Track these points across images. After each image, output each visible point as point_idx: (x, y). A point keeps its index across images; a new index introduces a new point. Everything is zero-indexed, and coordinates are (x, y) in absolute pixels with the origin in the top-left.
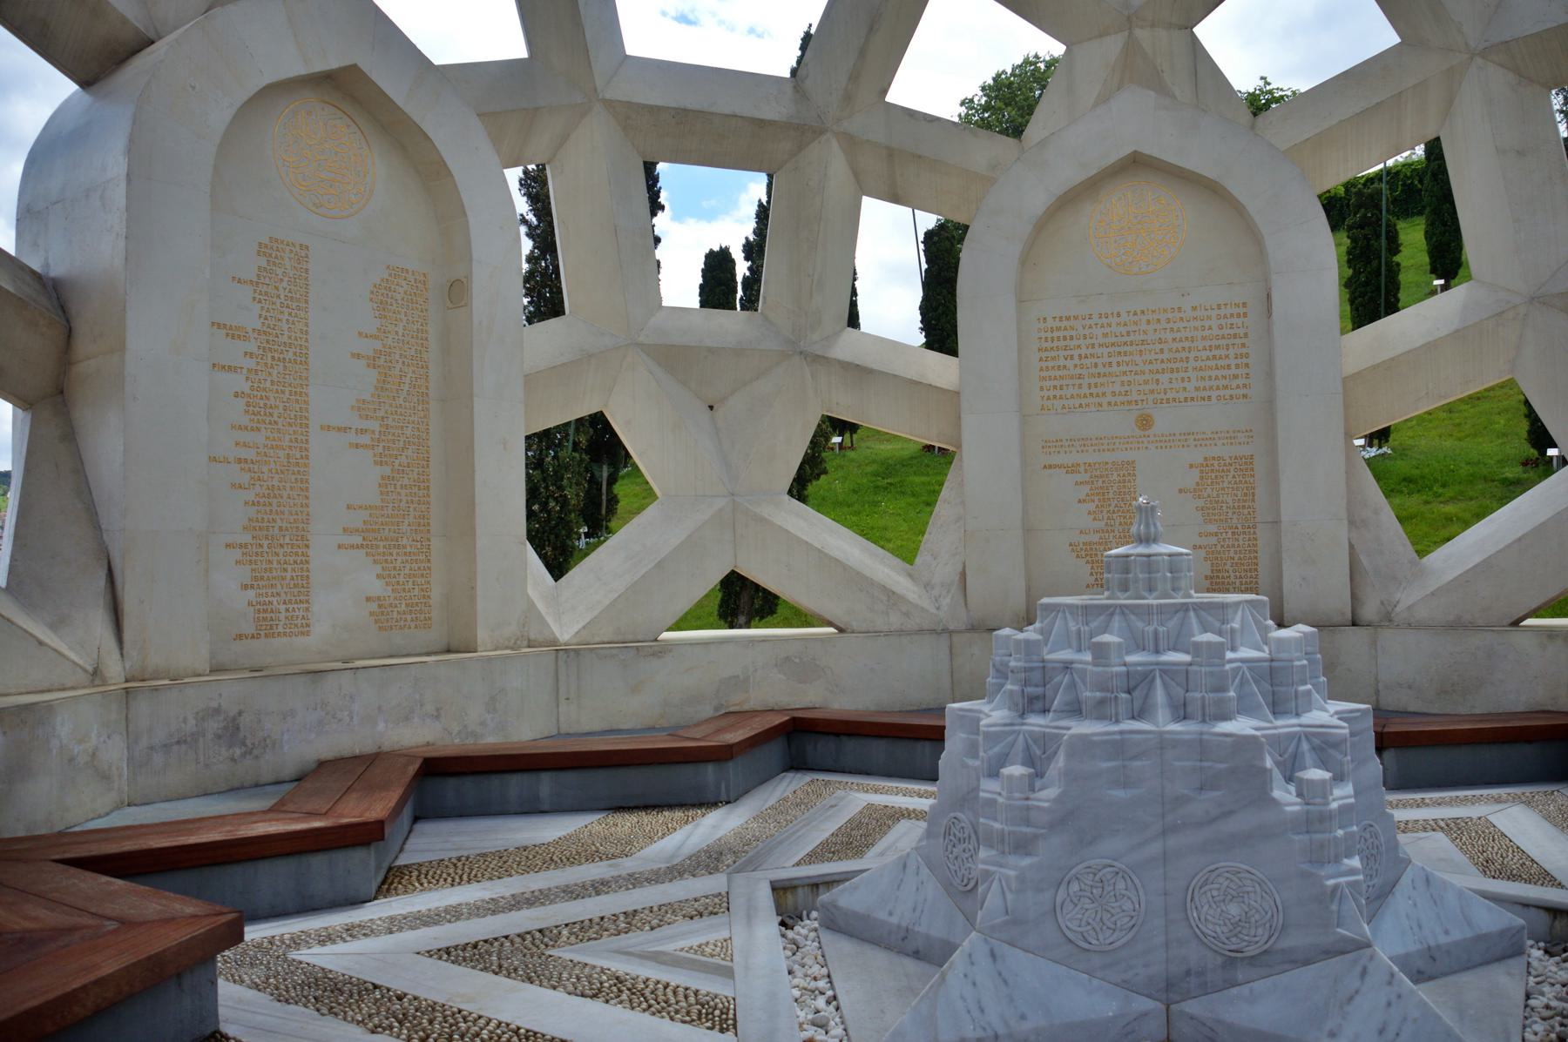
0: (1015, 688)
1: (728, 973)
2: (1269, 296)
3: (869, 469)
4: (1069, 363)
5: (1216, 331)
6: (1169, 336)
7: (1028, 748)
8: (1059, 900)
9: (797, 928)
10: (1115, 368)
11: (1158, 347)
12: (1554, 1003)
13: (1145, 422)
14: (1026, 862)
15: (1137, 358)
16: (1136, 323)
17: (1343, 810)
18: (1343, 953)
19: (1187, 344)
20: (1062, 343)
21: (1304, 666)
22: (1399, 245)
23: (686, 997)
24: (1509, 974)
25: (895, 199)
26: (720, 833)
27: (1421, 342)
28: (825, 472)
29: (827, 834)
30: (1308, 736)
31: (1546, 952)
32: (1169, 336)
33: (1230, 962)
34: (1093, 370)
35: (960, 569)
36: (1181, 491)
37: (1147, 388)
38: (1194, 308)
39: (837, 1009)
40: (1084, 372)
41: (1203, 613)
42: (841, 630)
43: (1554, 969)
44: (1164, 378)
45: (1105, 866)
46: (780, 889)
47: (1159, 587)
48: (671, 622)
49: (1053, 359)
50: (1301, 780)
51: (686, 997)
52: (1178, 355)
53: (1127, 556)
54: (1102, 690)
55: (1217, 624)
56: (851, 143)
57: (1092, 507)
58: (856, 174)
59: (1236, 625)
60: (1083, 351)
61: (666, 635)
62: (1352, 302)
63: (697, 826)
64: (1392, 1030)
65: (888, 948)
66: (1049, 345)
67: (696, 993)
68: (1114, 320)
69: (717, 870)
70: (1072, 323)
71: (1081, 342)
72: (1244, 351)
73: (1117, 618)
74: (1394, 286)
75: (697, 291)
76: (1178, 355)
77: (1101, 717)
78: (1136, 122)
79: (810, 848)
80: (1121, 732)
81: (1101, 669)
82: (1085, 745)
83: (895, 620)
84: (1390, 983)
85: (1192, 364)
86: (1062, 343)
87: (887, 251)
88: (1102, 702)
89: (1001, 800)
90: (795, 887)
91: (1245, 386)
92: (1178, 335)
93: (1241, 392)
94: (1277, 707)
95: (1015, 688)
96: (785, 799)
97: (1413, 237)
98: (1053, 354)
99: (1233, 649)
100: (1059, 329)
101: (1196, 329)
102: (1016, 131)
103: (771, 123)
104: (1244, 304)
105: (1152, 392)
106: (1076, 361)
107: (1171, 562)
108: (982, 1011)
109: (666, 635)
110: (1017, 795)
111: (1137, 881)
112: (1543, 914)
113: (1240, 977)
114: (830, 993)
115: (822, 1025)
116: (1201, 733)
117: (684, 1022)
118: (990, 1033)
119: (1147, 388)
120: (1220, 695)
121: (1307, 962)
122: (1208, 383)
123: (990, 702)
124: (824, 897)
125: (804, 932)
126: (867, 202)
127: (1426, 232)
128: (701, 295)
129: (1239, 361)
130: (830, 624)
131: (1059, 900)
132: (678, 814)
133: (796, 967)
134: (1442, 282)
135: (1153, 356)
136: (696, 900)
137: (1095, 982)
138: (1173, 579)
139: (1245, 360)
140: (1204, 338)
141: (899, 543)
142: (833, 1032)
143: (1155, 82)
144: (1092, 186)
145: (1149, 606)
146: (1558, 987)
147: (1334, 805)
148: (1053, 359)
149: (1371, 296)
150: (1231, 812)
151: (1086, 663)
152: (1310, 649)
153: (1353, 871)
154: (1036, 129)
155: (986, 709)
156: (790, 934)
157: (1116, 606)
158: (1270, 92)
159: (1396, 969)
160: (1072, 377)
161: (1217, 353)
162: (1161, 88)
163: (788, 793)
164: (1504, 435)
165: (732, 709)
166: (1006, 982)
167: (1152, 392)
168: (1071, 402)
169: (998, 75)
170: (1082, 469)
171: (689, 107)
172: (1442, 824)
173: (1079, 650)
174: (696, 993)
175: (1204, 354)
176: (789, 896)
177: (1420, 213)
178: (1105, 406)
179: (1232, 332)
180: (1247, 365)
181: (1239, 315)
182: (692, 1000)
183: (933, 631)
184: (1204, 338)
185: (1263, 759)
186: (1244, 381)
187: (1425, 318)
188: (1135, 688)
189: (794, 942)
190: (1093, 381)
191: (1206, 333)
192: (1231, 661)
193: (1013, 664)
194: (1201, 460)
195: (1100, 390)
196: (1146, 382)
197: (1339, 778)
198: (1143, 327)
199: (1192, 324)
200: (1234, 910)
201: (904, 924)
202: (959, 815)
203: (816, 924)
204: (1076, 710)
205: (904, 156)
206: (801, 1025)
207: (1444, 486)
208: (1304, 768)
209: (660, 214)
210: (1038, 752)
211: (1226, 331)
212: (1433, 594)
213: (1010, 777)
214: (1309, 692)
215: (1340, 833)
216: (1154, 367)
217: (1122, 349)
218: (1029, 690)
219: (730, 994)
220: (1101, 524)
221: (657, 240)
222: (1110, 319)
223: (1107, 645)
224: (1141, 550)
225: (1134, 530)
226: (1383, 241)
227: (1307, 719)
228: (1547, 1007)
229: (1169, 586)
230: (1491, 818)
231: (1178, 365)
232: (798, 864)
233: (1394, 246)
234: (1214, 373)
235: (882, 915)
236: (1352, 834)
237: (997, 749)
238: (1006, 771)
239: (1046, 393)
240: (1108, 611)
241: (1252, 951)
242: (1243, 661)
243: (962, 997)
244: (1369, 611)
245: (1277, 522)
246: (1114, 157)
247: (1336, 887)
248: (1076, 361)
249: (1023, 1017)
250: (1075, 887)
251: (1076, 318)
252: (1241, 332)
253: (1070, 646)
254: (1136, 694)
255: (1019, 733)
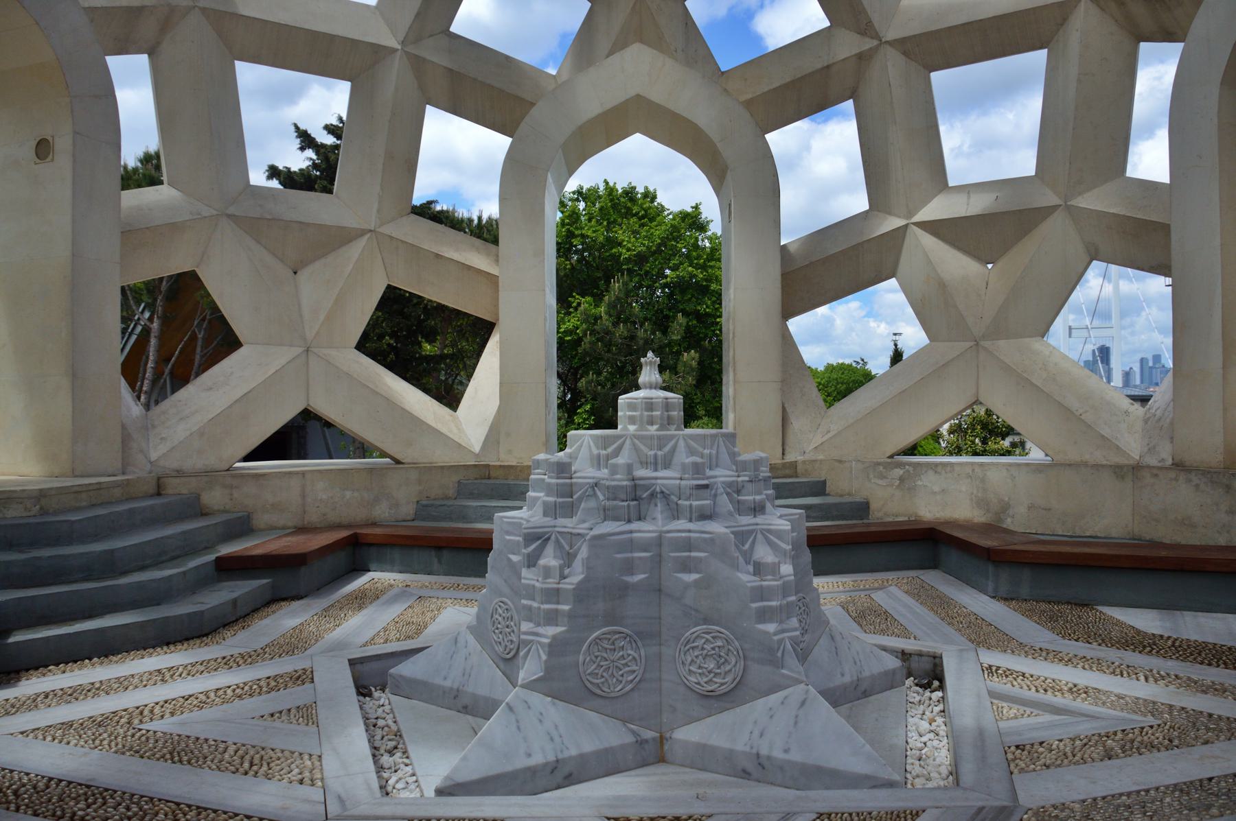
48: (244, 453)
61: (238, 465)
64: (555, 734)
83: (1099, 456)
89: (537, 584)
108: (761, 735)
109: (238, 465)
118: (754, 751)
126: (430, 111)
130: (383, 454)
143: (658, 43)
201: (455, 687)
235: (438, 681)
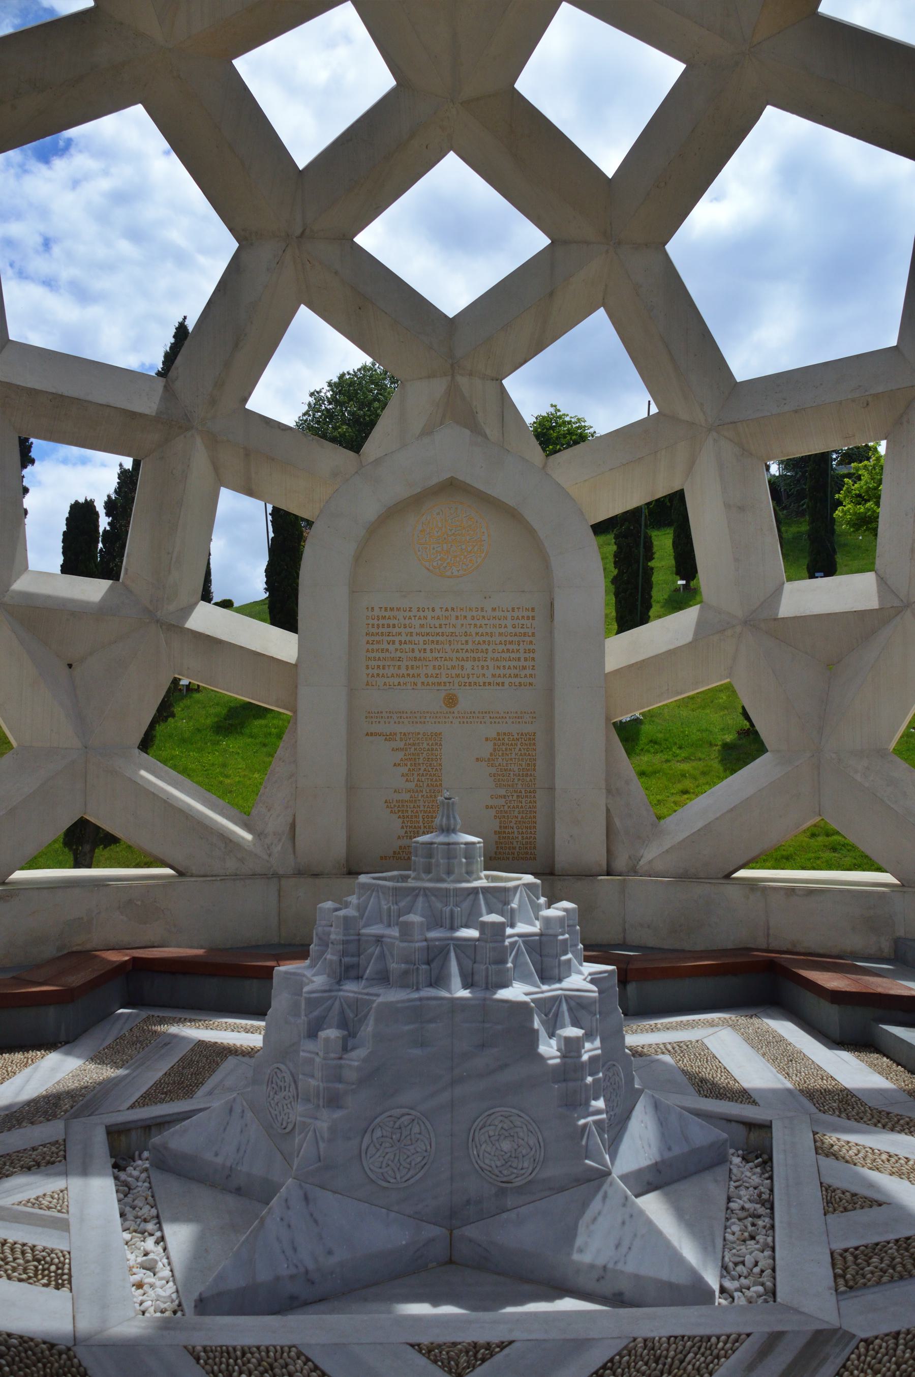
0: (335, 958)
1: (63, 1226)
2: (552, 604)
3: (212, 711)
4: (391, 648)
5: (510, 629)
6: (473, 630)
7: (342, 1012)
8: (364, 1147)
9: (130, 1169)
10: (428, 654)
11: (464, 639)
12: (747, 1206)
13: (451, 701)
14: (338, 1114)
15: (447, 646)
16: (447, 618)
17: (592, 1059)
18: (589, 1181)
19: (487, 638)
20: (385, 630)
21: (566, 940)
22: (653, 554)
23: (23, 1253)
24: (716, 1181)
25: (250, 493)
26: (59, 1076)
27: (664, 649)
28: (173, 715)
29: (161, 1074)
30: (567, 998)
31: (743, 1158)
32: (473, 630)
33: (502, 1193)
34: (410, 655)
35: (290, 820)
36: (477, 759)
37: (454, 672)
38: (494, 610)
39: (165, 1249)
40: (403, 655)
41: (489, 896)
42: (181, 874)
43: (748, 1174)
44: (468, 665)
45: (403, 1115)
46: (114, 1133)
47: (456, 871)
49: (378, 642)
50: (560, 1036)
51: (23, 1253)
52: (480, 647)
53: (432, 843)
54: (406, 962)
55: (500, 906)
56: (213, 441)
57: (404, 770)
58: (216, 468)
59: (514, 905)
60: (403, 638)
62: (617, 595)
63: (36, 1069)
65: (213, 1185)
66: (375, 630)
67: (33, 1248)
68: (429, 614)
69: (55, 1116)
70: (395, 613)
71: (402, 630)
72: (531, 647)
73: (421, 899)
74: (647, 605)
75: (61, 550)
76: (480, 647)
77: (404, 986)
78: (453, 453)
79: (144, 1090)
80: (421, 999)
81: (405, 944)
82: (391, 1012)
83: (231, 865)
84: (624, 1205)
85: (490, 655)
86: (385, 630)
87: (237, 544)
88: (406, 973)
90: (129, 1130)
91: (531, 676)
92: (480, 630)
93: (528, 680)
94: (545, 976)
95: (335, 958)
96: (122, 1038)
97: (663, 542)
98: (377, 638)
99: (512, 926)
100: (384, 618)
101: (495, 626)
102: (355, 444)
103: (142, 415)
104: (533, 610)
105: (458, 676)
106: (397, 645)
107: (466, 849)
110: (332, 1055)
111: (429, 1127)
112: (741, 1128)
113: (509, 1203)
114: (158, 1234)
115: (151, 1268)
116: (485, 999)
117: (20, 1280)
119: (454, 672)
120: (500, 967)
121: (562, 1190)
122: (502, 672)
123: (312, 966)
124: (156, 1140)
125: (136, 1173)
127: (674, 543)
128: (63, 541)
129: (527, 655)
131: (364, 1147)
132: (18, 1056)
133: (128, 1209)
134: (684, 582)
135: (460, 646)
136: (34, 1149)
137: (393, 1214)
138: (468, 864)
139: (532, 655)
140: (500, 634)
141: (237, 779)
142: (160, 1275)
144: (417, 501)
145: (447, 890)
146: (751, 1189)
147: (585, 1057)
148: (378, 642)
149: (631, 609)
150: (506, 1065)
151: (395, 938)
152: (571, 922)
153: (598, 1112)
154: (373, 446)
155: (308, 973)
156: (123, 1176)
157: (420, 889)
158: (560, 417)
159: (629, 1193)
160: (393, 659)
161: (511, 647)
162: (475, 428)
163: (125, 1031)
164: (726, 708)
165: (74, 949)
166: (316, 1222)
167: (458, 676)
168: (391, 680)
169: (343, 375)
170: (398, 738)
171: (66, 393)
172: (669, 1047)
173: (389, 926)
174: (33, 1248)
175: (500, 648)
176: (123, 1138)
177: (669, 525)
178: (419, 685)
179: (522, 631)
180: (533, 659)
181: (528, 618)
182: (29, 1256)
183: (264, 876)
184: (500, 634)
185: (532, 1022)
186: (531, 672)
187: (666, 631)
188: (433, 960)
189: (126, 1184)
190: (410, 663)
191: (503, 630)
192: (511, 936)
193: (333, 937)
194: (494, 735)
195: (416, 672)
196: (453, 667)
197: (589, 1036)
198: (453, 621)
199: (492, 622)
200: (506, 1145)
202: (282, 1067)
203: (147, 1165)
204: (384, 978)
205: (255, 451)
206: (131, 1268)
207: (680, 748)
208: (563, 1026)
209: (30, 468)
210: (351, 1015)
211: (518, 630)
212: (667, 851)
213: (327, 1040)
214: (569, 961)
215: (589, 1079)
216: (460, 655)
217: (435, 638)
218: (346, 960)
219: (65, 1248)
220: (411, 785)
221: (26, 491)
222: (426, 613)
223: (413, 923)
224: (442, 839)
225: (437, 821)
226: (642, 550)
227: (566, 984)
228: (743, 1208)
229: (464, 870)
230: (706, 1041)
231: (480, 655)
232: (132, 1107)
233: (649, 554)
234: (507, 664)
235: (209, 1156)
236: (599, 1079)
237: (316, 1013)
238: (323, 1034)
239: (370, 671)
240: (415, 892)
241: (518, 1182)
242: (520, 935)
243: (278, 1239)
244: (621, 863)
245: (552, 789)
246: (435, 481)
247: (585, 1125)
248: (397, 645)
249: (330, 1253)
250: (378, 1133)
251: (398, 609)
252: (530, 631)
253: (381, 922)
254: (434, 965)
255: (336, 998)
